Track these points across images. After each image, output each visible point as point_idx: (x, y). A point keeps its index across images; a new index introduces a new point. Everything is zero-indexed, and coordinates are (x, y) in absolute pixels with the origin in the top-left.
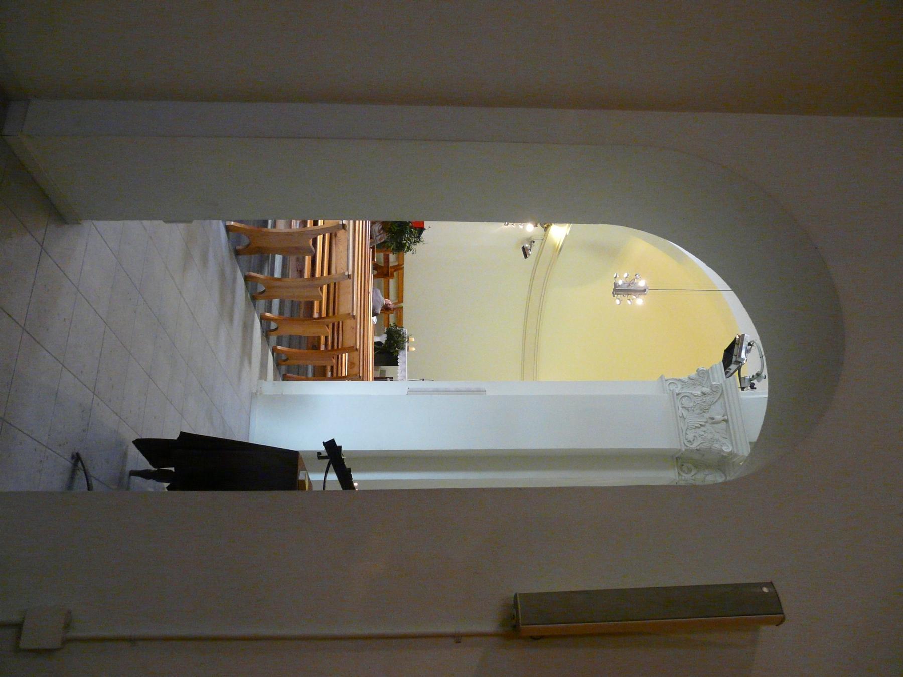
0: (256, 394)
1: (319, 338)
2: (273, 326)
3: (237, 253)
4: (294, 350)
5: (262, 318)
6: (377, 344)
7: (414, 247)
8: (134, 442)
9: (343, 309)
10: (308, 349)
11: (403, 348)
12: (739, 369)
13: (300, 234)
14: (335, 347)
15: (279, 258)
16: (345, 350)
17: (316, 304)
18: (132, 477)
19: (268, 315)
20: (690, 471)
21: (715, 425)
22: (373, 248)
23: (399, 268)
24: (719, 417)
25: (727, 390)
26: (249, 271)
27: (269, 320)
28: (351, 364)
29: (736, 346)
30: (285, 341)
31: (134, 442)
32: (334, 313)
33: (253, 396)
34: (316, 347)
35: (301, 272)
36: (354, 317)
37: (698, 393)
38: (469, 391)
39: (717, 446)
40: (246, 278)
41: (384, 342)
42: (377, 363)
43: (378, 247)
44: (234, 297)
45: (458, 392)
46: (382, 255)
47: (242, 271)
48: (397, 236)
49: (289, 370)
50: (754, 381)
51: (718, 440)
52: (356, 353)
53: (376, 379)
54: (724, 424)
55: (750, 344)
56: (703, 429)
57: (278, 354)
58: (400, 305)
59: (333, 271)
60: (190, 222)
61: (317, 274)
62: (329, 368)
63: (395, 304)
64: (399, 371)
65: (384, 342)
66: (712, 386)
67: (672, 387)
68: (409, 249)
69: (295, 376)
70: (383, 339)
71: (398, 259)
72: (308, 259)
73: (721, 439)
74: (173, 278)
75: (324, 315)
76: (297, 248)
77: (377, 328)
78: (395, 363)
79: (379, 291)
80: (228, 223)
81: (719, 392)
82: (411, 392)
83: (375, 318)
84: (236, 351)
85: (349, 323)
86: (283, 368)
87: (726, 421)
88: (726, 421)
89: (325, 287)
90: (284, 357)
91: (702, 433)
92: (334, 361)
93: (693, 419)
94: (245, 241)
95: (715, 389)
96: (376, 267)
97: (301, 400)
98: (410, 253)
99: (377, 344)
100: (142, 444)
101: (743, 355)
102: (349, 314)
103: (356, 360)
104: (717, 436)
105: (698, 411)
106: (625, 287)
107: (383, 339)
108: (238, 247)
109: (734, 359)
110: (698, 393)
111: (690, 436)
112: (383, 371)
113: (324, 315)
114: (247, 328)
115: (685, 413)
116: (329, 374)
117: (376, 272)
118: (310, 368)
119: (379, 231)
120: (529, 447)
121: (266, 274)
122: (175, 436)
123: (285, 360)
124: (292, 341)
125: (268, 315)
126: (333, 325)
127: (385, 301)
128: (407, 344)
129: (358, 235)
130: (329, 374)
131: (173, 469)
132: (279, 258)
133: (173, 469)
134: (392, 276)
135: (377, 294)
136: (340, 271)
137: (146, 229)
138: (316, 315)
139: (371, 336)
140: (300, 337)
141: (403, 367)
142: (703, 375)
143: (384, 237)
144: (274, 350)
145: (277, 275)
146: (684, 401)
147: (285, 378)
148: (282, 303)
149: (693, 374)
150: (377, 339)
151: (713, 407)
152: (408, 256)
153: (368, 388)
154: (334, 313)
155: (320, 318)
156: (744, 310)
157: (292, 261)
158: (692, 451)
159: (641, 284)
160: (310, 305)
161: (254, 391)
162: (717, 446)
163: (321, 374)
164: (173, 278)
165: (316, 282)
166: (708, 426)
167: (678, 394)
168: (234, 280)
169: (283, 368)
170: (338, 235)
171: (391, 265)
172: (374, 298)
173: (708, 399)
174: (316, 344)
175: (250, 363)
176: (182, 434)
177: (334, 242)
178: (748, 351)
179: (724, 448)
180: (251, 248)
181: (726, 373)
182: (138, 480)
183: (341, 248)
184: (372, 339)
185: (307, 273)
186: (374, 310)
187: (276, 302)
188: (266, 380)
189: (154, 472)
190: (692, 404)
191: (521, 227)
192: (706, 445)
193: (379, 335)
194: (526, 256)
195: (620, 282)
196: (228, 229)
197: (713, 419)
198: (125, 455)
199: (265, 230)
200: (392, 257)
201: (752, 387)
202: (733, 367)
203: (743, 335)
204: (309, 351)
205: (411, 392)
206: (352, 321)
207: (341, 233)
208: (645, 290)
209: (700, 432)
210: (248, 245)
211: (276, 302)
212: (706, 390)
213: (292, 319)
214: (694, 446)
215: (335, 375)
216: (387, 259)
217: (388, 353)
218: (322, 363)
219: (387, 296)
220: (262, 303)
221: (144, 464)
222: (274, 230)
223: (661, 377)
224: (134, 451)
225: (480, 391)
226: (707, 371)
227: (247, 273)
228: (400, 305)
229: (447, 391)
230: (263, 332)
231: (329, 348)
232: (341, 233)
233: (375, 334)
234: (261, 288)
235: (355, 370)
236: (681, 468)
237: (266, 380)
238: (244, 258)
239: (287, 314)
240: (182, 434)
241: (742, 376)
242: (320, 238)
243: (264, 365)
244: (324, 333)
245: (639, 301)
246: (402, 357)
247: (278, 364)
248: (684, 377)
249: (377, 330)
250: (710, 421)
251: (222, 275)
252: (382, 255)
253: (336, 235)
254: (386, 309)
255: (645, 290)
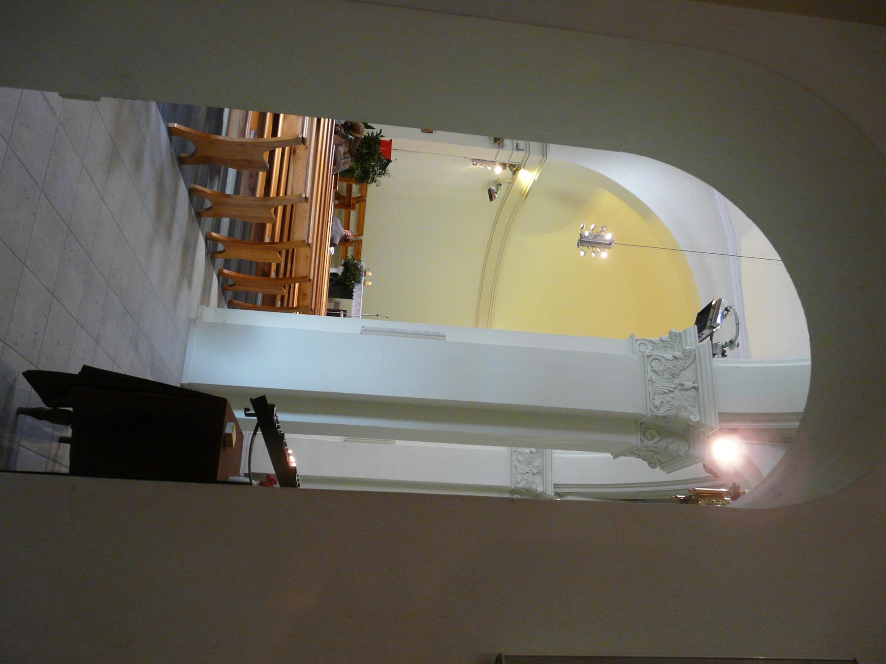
0: (195, 320)
1: (270, 264)
2: (220, 247)
3: (181, 161)
4: (241, 275)
5: (207, 238)
6: (333, 276)
7: (379, 178)
8: (24, 374)
9: (298, 234)
10: (256, 275)
11: (359, 282)
12: (711, 335)
13: (254, 145)
14: (288, 276)
15: (232, 173)
16: (296, 280)
17: (269, 227)
18: (21, 416)
19: (214, 234)
20: (653, 438)
21: (683, 392)
22: (336, 175)
23: (362, 199)
24: (689, 384)
25: (700, 356)
26: (195, 183)
27: (216, 241)
28: (302, 295)
29: (712, 310)
30: (234, 265)
31: (24, 374)
32: (289, 239)
33: (192, 322)
34: (266, 274)
35: (253, 190)
36: (308, 245)
37: (670, 356)
38: (427, 335)
39: (683, 414)
40: (191, 192)
41: (340, 274)
42: (332, 294)
43: (343, 175)
44: (174, 210)
45: (415, 335)
46: (345, 184)
47: (185, 182)
48: (364, 158)
49: (236, 296)
50: (727, 349)
51: (685, 408)
52: (309, 284)
53: (328, 315)
54: (692, 393)
55: (726, 309)
56: (671, 395)
57: (224, 278)
58: (359, 238)
59: (289, 192)
60: (98, 99)
61: (273, 193)
62: (279, 297)
63: (355, 236)
64: (354, 305)
65: (340, 274)
66: (684, 351)
67: (643, 348)
68: (373, 180)
69: (243, 303)
70: (339, 270)
71: (360, 190)
72: (262, 176)
73: (689, 407)
74: (91, 178)
75: (277, 239)
76: (249, 161)
77: (333, 258)
78: (350, 296)
79: (339, 221)
80: (171, 125)
81: (690, 356)
82: (365, 331)
83: (332, 248)
84: (174, 271)
85: (303, 252)
86: (229, 294)
87: (696, 388)
88: (696, 388)
89: (280, 209)
90: (231, 282)
91: (670, 399)
92: (286, 291)
93: (662, 384)
94: (191, 147)
95: (687, 354)
96: (337, 196)
97: (245, 331)
98: (374, 184)
99: (333, 276)
100: (33, 377)
101: (719, 321)
102: (304, 241)
103: (308, 291)
104: (686, 404)
105: (666, 376)
106: (591, 239)
107: (339, 270)
108: (183, 155)
109: (708, 324)
110: (670, 356)
111: (657, 403)
112: (337, 304)
113: (277, 239)
114: (188, 248)
115: (654, 376)
116: (279, 304)
117: (337, 202)
118: (260, 296)
119: (345, 154)
120: (486, 401)
121: (215, 189)
122: (76, 370)
123: (231, 286)
124: (240, 266)
125: (214, 234)
126: (287, 251)
127: (345, 232)
128: (363, 278)
129: (314, 135)
130: (279, 304)
131: (71, 409)
132: (232, 173)
133: (71, 409)
134: (354, 208)
135: (336, 224)
136: (297, 192)
137: (55, 114)
138: (267, 239)
139: (328, 268)
140: (251, 262)
141: (356, 303)
142: (676, 337)
143: (347, 164)
144: (220, 274)
145: (229, 190)
146: (654, 363)
147: (231, 305)
148: (232, 224)
149: (665, 336)
150: (333, 270)
151: (683, 372)
152: (371, 187)
153: (320, 323)
154: (289, 239)
155: (273, 242)
156: (787, 275)
157: (245, 174)
158: (657, 417)
159: (608, 237)
160: (262, 228)
161: (193, 316)
162: (684, 414)
163: (269, 304)
164: (91, 178)
165: (269, 203)
166: (677, 392)
167: (648, 356)
168: (176, 188)
169: (229, 294)
170: (298, 152)
171: (353, 195)
172: (333, 227)
173: (679, 363)
174: (266, 270)
175: (190, 286)
176: (85, 368)
177: (292, 164)
178: (723, 317)
179: (691, 417)
180: (199, 155)
181: (699, 337)
182: (30, 419)
183: (300, 166)
184: (327, 270)
185: (259, 192)
186: (332, 240)
187: (226, 221)
188: (208, 306)
189: (48, 410)
190: (662, 368)
191: (489, 168)
192: (672, 412)
193: (336, 267)
194: (491, 199)
195: (587, 234)
196: (171, 131)
197: (682, 385)
198: (11, 389)
199: (219, 138)
200: (355, 188)
201: (723, 354)
202: (706, 332)
203: (720, 300)
204: (260, 279)
205: (365, 331)
206: (308, 249)
207: (300, 149)
208: (610, 244)
209: (667, 398)
210: (195, 153)
211: (226, 221)
212: (679, 354)
213: (243, 241)
214: (661, 412)
215: (285, 305)
216: (349, 189)
217: (343, 285)
218: (273, 291)
219: (347, 227)
220: (208, 221)
221: (36, 401)
222: (228, 139)
223: (632, 336)
224: (24, 385)
225: (439, 336)
226: (680, 334)
227: (192, 186)
228: (359, 238)
229: (404, 334)
230: (207, 253)
231: (281, 276)
232: (300, 149)
233: (331, 266)
234: (208, 204)
235: (307, 302)
236: (644, 434)
237: (208, 306)
238: (189, 168)
239: (238, 235)
240: (85, 368)
241: (714, 342)
242: (278, 151)
243: (206, 290)
244: (276, 260)
245: (604, 254)
246: (358, 291)
247: (223, 289)
248: (656, 339)
249: (334, 260)
250: (680, 387)
251: (160, 185)
252: (345, 184)
253: (295, 152)
254: (345, 240)
255: (610, 244)
